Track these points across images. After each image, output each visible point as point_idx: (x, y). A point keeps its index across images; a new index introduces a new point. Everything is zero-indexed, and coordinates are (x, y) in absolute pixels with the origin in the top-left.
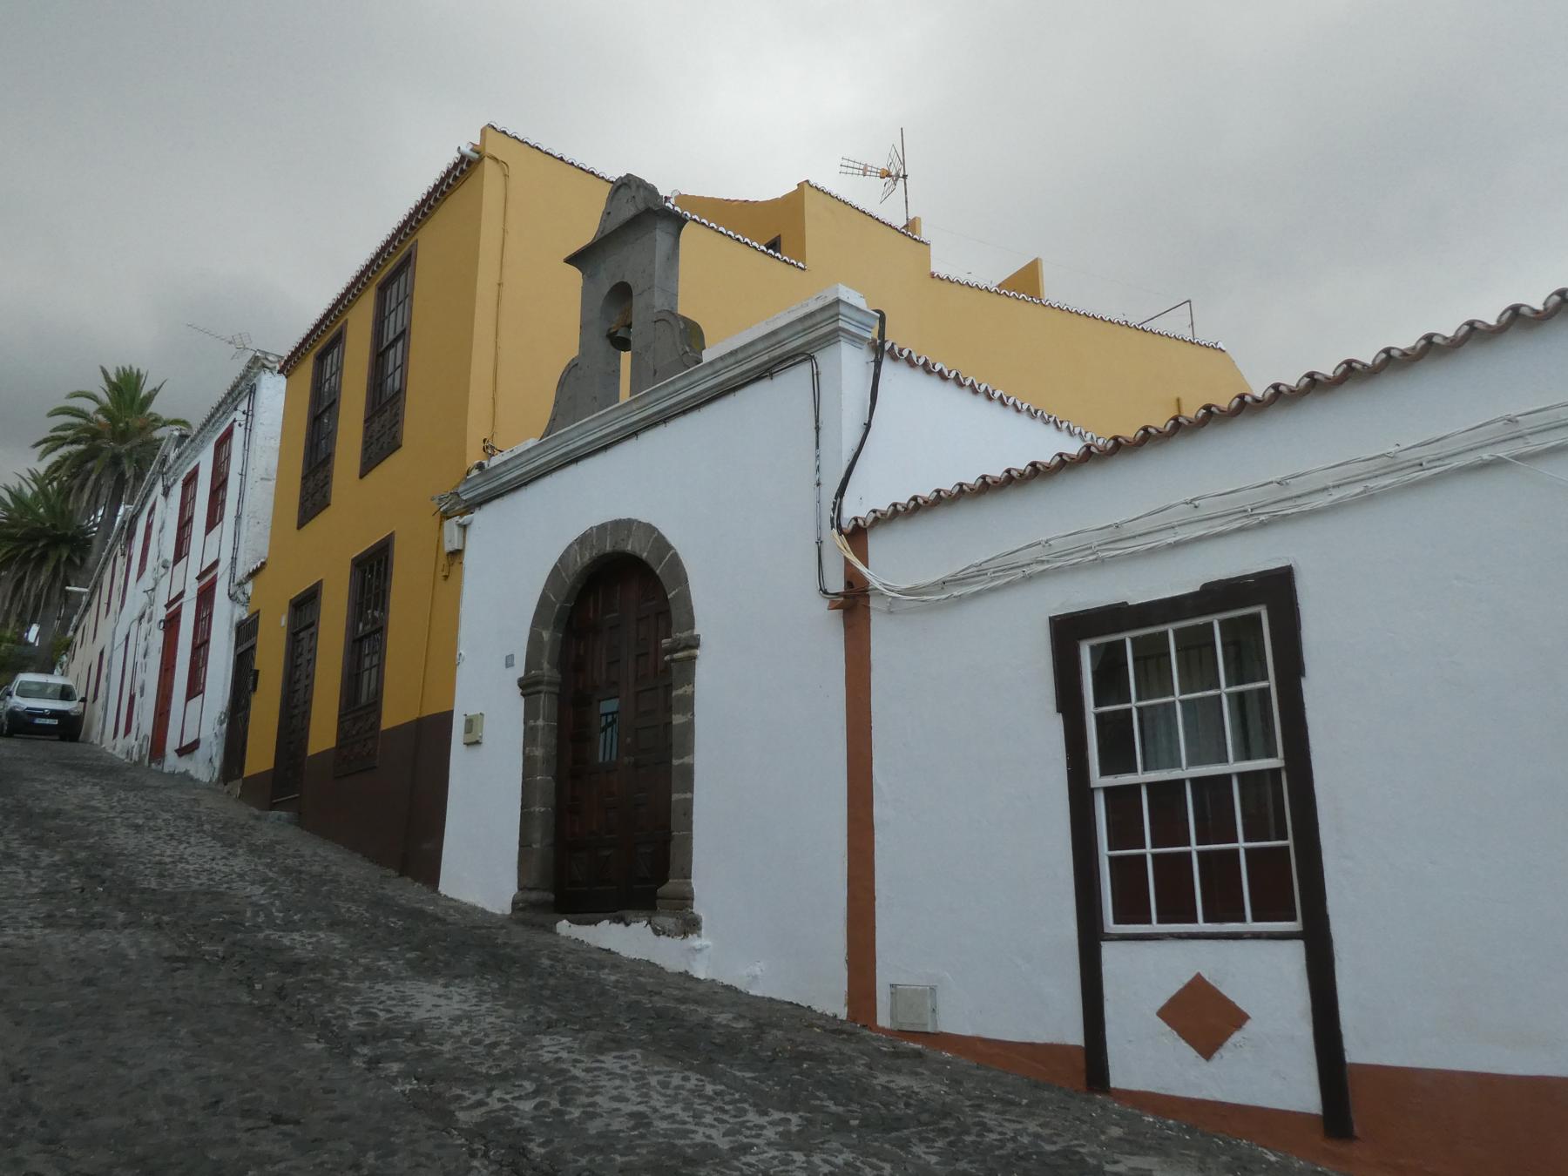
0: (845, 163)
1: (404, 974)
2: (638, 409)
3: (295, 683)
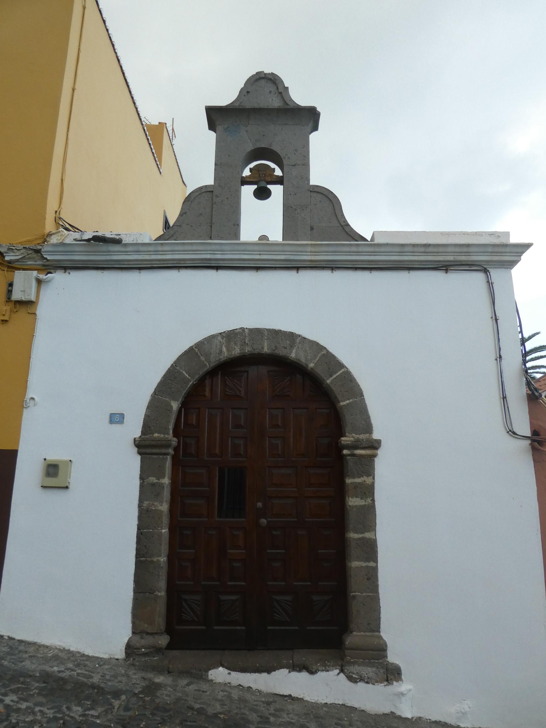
2: (311, 252)
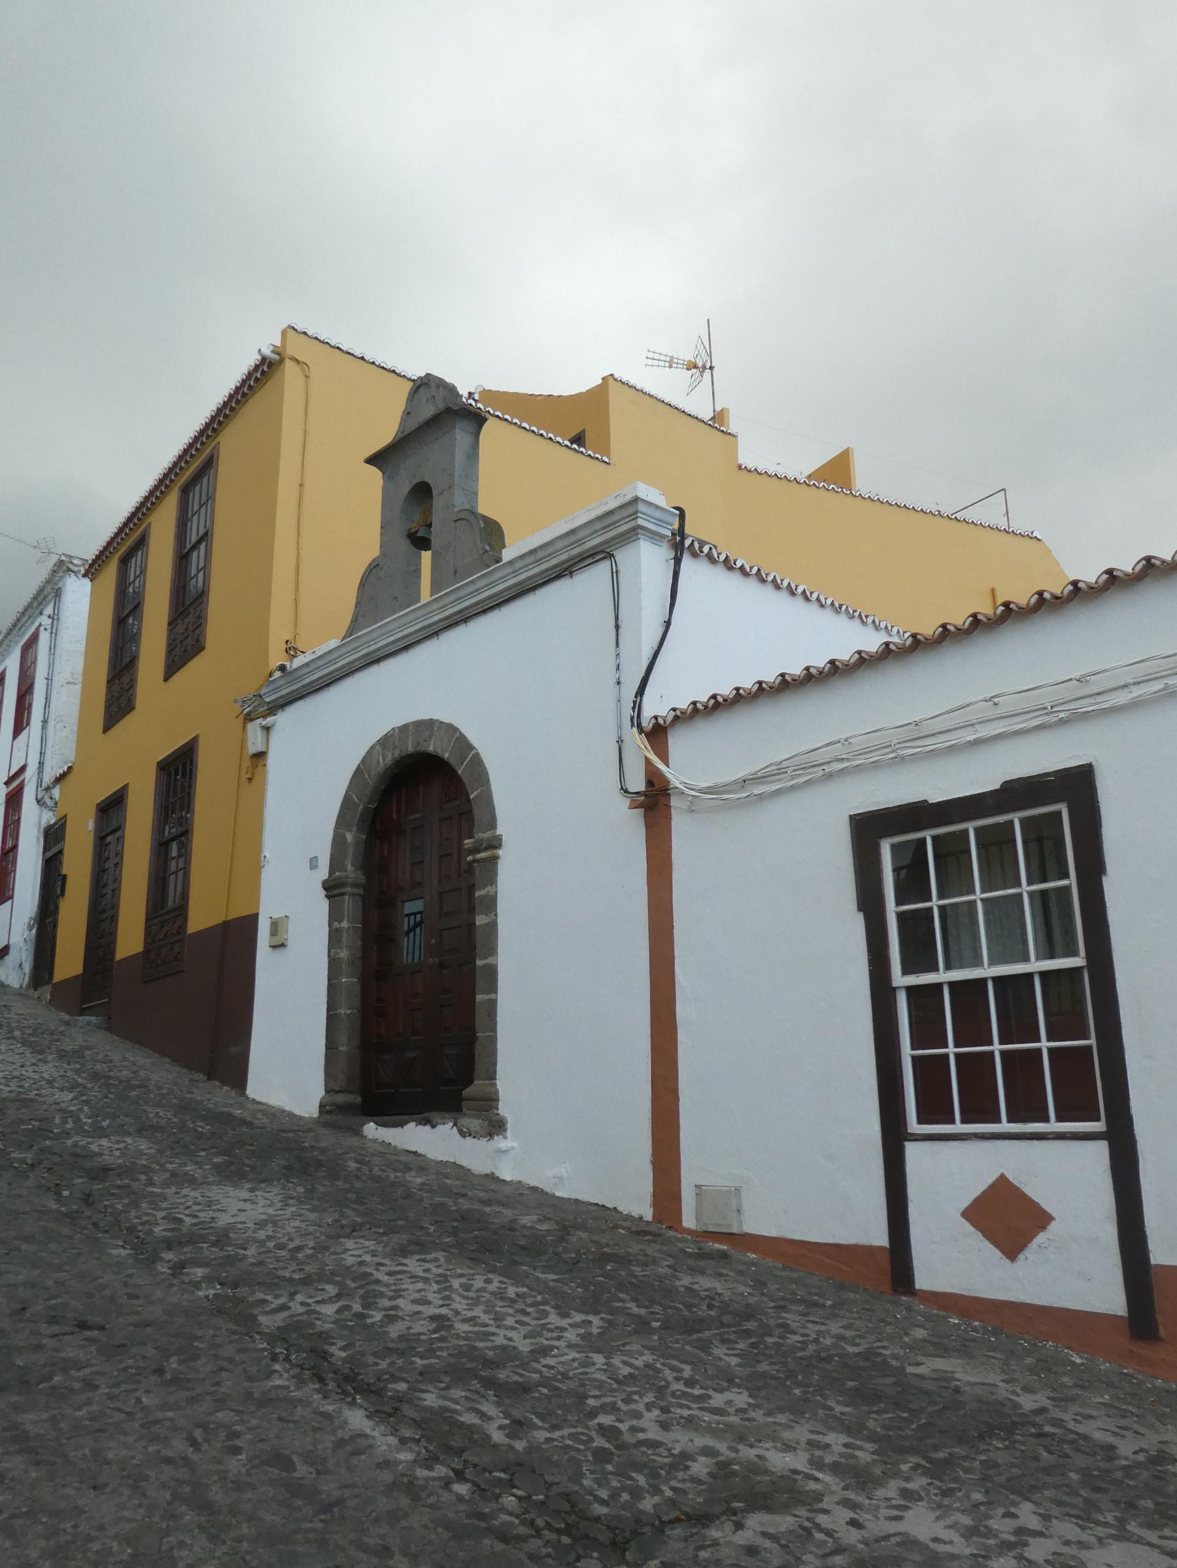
0: (651, 355)
1: (211, 1179)
2: (438, 609)
3: (103, 887)
